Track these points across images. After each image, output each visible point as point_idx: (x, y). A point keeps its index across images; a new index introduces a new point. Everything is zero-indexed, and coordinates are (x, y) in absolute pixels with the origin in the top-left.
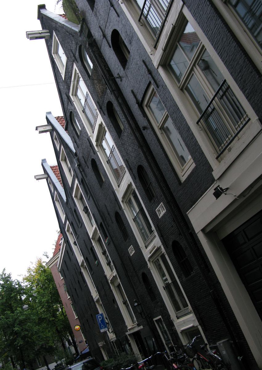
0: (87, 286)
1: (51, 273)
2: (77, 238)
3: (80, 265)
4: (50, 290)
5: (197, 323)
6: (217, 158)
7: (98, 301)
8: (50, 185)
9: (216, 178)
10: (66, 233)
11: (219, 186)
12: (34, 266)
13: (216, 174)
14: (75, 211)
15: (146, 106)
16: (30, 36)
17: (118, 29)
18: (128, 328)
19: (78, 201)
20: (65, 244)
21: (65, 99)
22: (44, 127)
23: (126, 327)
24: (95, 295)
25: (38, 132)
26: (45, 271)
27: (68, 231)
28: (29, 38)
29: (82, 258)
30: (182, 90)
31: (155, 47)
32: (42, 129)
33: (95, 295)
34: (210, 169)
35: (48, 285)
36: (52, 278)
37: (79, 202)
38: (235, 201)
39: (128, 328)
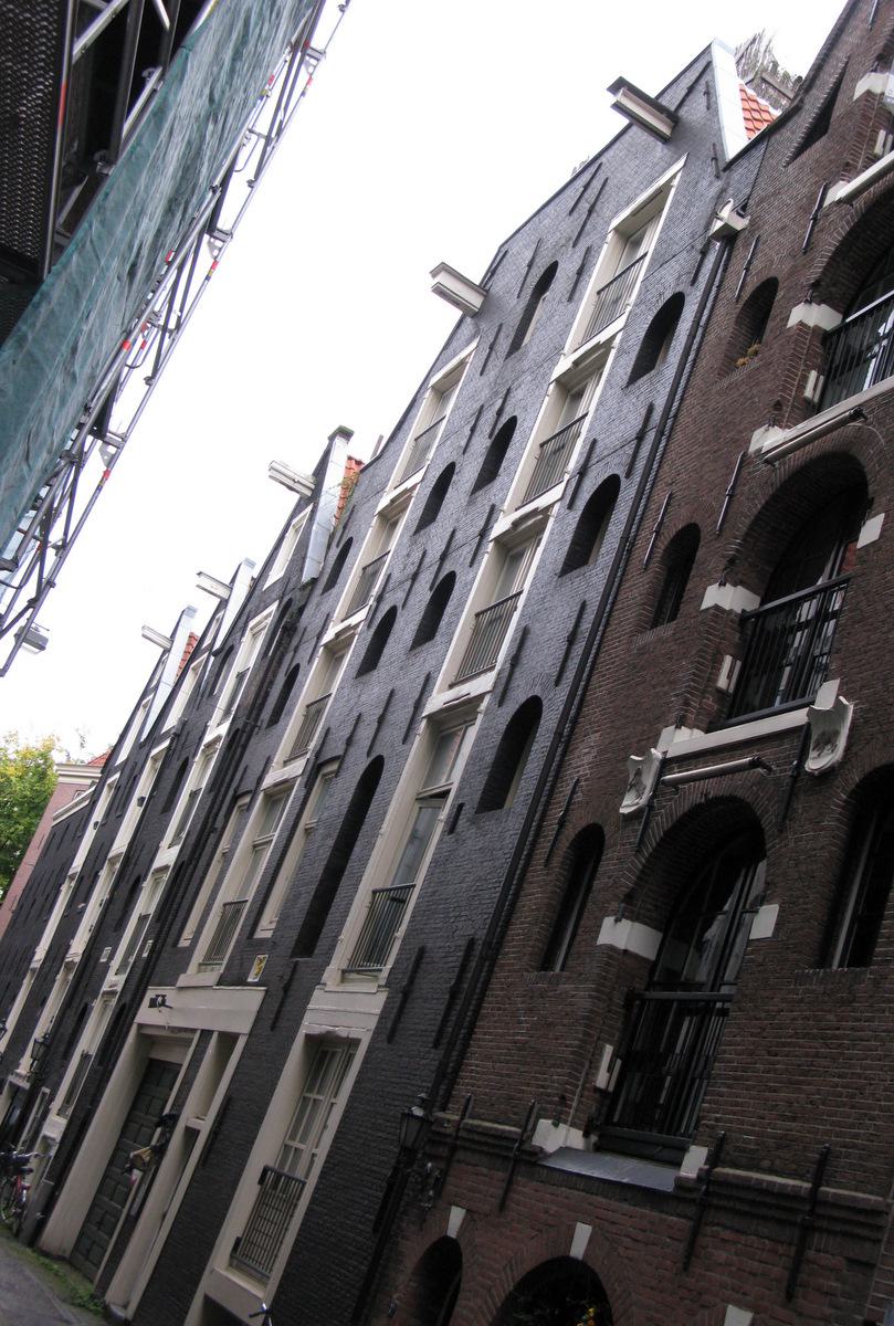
0: (46, 921)
1: (51, 795)
2: (151, 796)
3: (111, 855)
4: (12, 830)
5: (58, 1140)
6: (344, 972)
7: (34, 970)
8: (291, 531)
9: (179, 984)
10: (104, 786)
11: (164, 996)
12: (31, 740)
13: (183, 980)
14: (135, 778)
15: (324, 775)
16: (444, 279)
17: (457, 573)
18: (18, 1071)
19: (151, 771)
20: (87, 803)
21: (240, 624)
22: (214, 584)
23: (17, 1066)
24: (40, 953)
25: (612, 99)
26: (42, 776)
27: (155, 759)
28: (438, 279)
29: (124, 850)
30: (255, 846)
31: (451, 686)
32: (207, 584)
33: (40, 953)
34: (184, 970)
35: (20, 815)
36: (43, 808)
37: (149, 773)
38: (163, 1027)
39: (18, 1071)
